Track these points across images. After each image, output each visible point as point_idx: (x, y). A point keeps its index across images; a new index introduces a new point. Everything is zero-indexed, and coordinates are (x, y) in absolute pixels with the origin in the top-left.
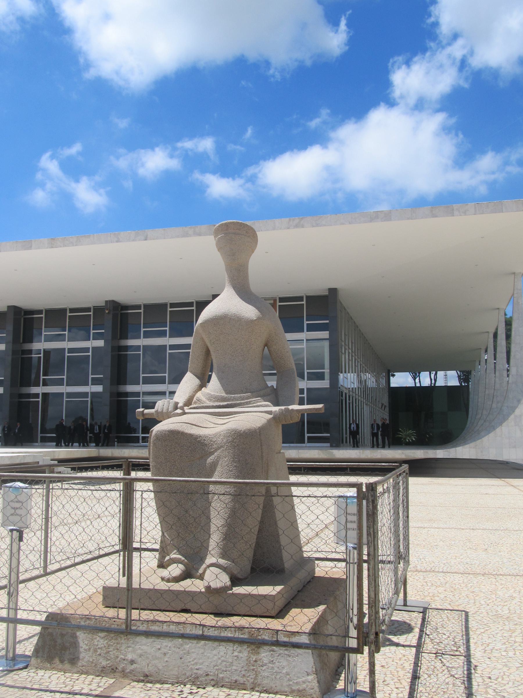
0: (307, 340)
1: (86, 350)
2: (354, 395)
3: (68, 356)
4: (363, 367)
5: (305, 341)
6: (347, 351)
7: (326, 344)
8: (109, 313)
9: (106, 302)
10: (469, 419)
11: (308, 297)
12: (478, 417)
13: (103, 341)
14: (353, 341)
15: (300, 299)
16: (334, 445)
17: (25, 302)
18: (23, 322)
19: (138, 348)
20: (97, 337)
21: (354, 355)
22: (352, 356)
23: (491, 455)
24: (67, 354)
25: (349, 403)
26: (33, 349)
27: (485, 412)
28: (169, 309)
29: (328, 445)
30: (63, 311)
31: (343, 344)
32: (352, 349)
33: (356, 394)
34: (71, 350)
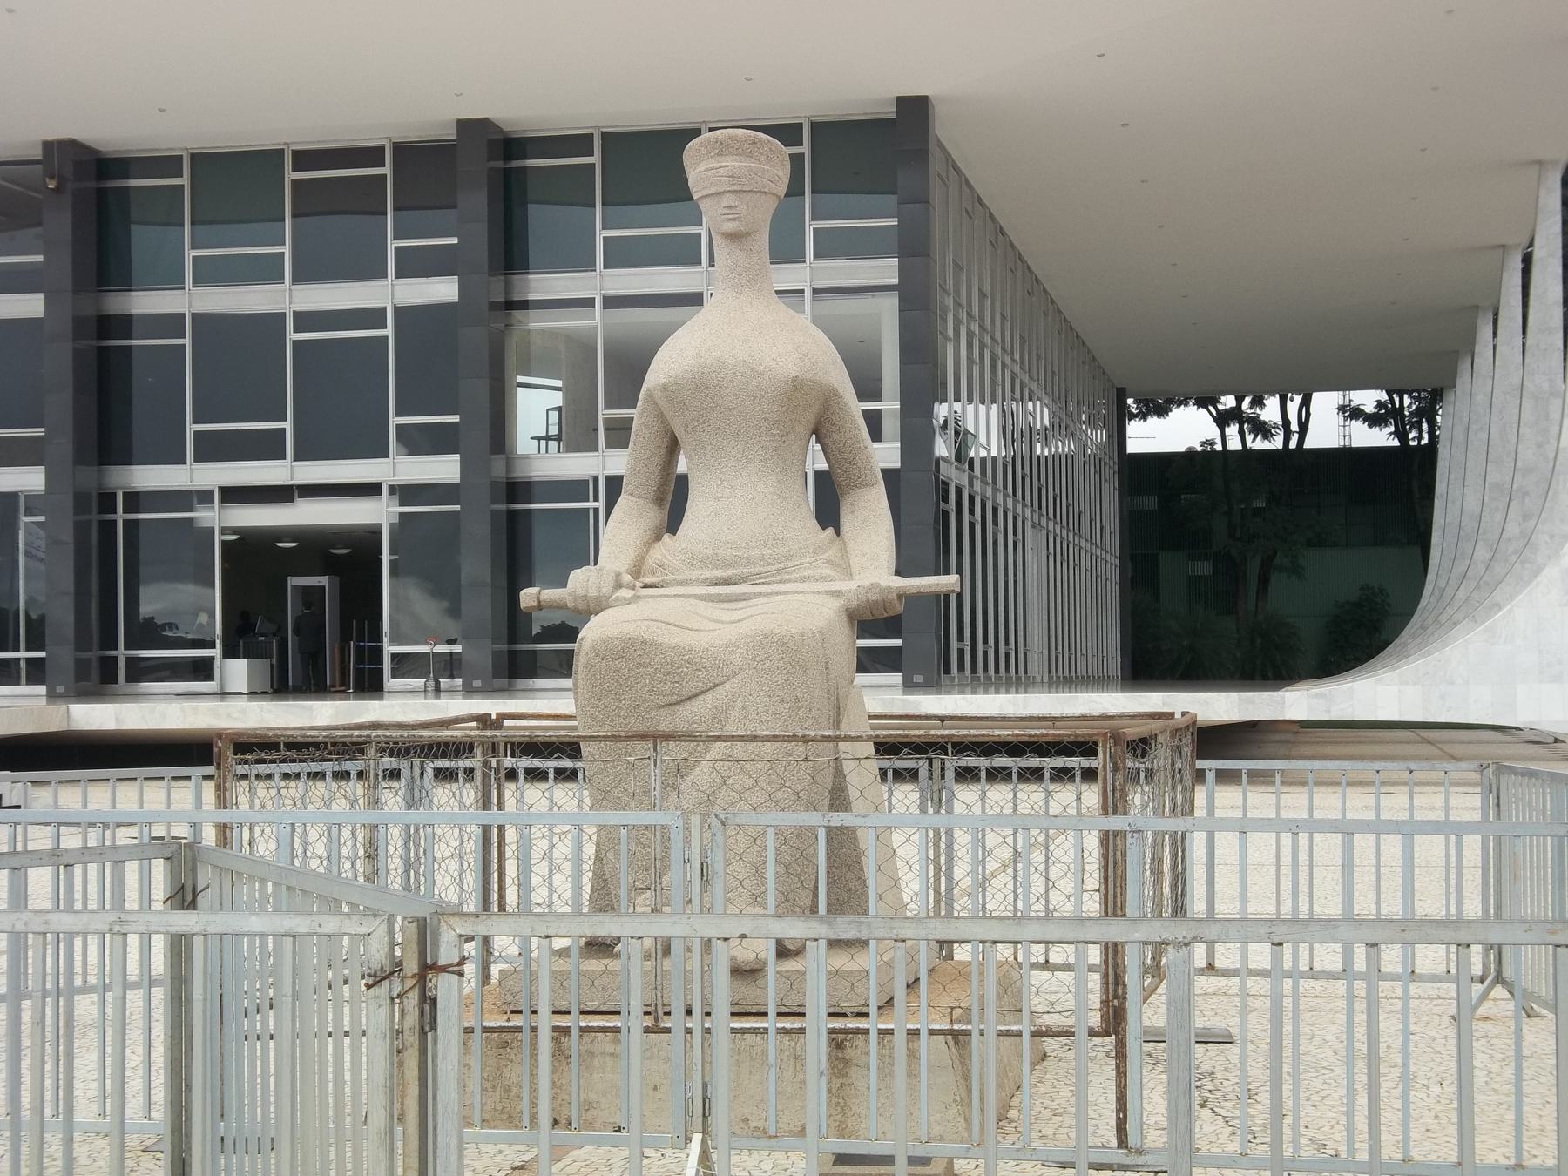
0: (816, 291)
1: (373, 317)
2: (989, 493)
3: (295, 343)
4: (1022, 384)
5: (808, 294)
6: (963, 331)
7: (889, 306)
8: (57, 190)
9: (47, 146)
10: (1431, 577)
11: (401, 150)
12: (1460, 569)
13: (41, 296)
14: (987, 289)
15: (372, 155)
16: (918, 679)
17: (111, 127)
18: (96, 202)
19: (173, 323)
20: (414, 265)
21: (988, 340)
22: (982, 346)
23: (1474, 705)
24: (292, 336)
25: (972, 525)
26: (134, 311)
27: (1482, 553)
28: (290, 175)
29: (897, 678)
30: (265, 162)
31: (950, 302)
32: (982, 319)
33: (995, 490)
34: (305, 320)
